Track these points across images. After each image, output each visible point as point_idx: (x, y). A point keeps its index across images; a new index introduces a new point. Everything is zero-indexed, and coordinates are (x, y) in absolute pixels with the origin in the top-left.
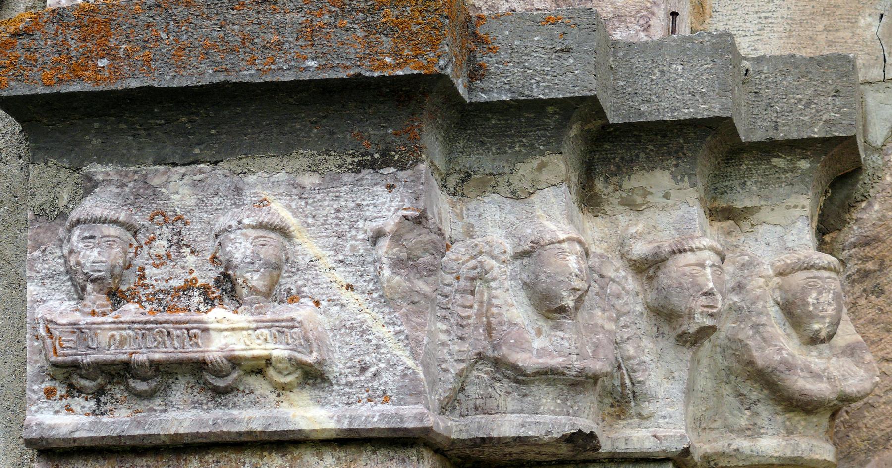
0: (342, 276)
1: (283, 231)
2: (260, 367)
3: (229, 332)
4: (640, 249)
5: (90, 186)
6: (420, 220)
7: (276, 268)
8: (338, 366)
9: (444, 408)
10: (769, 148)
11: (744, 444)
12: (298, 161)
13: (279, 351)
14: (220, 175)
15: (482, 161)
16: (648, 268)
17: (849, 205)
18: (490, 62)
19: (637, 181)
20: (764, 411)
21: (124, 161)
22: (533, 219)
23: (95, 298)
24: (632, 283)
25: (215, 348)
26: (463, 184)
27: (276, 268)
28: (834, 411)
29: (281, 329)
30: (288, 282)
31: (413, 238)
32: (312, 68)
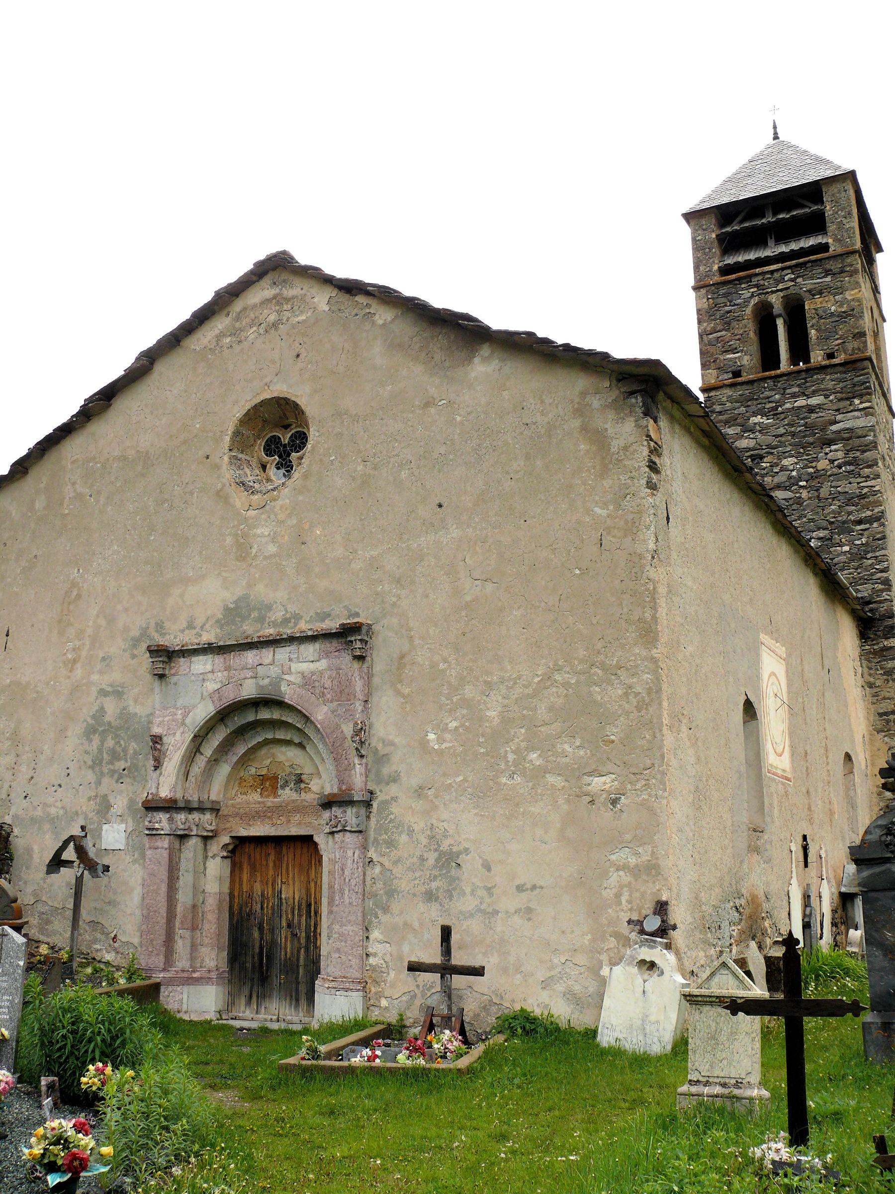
3: (157, 826)
22: (181, 817)
26: (177, 813)
28: (212, 831)
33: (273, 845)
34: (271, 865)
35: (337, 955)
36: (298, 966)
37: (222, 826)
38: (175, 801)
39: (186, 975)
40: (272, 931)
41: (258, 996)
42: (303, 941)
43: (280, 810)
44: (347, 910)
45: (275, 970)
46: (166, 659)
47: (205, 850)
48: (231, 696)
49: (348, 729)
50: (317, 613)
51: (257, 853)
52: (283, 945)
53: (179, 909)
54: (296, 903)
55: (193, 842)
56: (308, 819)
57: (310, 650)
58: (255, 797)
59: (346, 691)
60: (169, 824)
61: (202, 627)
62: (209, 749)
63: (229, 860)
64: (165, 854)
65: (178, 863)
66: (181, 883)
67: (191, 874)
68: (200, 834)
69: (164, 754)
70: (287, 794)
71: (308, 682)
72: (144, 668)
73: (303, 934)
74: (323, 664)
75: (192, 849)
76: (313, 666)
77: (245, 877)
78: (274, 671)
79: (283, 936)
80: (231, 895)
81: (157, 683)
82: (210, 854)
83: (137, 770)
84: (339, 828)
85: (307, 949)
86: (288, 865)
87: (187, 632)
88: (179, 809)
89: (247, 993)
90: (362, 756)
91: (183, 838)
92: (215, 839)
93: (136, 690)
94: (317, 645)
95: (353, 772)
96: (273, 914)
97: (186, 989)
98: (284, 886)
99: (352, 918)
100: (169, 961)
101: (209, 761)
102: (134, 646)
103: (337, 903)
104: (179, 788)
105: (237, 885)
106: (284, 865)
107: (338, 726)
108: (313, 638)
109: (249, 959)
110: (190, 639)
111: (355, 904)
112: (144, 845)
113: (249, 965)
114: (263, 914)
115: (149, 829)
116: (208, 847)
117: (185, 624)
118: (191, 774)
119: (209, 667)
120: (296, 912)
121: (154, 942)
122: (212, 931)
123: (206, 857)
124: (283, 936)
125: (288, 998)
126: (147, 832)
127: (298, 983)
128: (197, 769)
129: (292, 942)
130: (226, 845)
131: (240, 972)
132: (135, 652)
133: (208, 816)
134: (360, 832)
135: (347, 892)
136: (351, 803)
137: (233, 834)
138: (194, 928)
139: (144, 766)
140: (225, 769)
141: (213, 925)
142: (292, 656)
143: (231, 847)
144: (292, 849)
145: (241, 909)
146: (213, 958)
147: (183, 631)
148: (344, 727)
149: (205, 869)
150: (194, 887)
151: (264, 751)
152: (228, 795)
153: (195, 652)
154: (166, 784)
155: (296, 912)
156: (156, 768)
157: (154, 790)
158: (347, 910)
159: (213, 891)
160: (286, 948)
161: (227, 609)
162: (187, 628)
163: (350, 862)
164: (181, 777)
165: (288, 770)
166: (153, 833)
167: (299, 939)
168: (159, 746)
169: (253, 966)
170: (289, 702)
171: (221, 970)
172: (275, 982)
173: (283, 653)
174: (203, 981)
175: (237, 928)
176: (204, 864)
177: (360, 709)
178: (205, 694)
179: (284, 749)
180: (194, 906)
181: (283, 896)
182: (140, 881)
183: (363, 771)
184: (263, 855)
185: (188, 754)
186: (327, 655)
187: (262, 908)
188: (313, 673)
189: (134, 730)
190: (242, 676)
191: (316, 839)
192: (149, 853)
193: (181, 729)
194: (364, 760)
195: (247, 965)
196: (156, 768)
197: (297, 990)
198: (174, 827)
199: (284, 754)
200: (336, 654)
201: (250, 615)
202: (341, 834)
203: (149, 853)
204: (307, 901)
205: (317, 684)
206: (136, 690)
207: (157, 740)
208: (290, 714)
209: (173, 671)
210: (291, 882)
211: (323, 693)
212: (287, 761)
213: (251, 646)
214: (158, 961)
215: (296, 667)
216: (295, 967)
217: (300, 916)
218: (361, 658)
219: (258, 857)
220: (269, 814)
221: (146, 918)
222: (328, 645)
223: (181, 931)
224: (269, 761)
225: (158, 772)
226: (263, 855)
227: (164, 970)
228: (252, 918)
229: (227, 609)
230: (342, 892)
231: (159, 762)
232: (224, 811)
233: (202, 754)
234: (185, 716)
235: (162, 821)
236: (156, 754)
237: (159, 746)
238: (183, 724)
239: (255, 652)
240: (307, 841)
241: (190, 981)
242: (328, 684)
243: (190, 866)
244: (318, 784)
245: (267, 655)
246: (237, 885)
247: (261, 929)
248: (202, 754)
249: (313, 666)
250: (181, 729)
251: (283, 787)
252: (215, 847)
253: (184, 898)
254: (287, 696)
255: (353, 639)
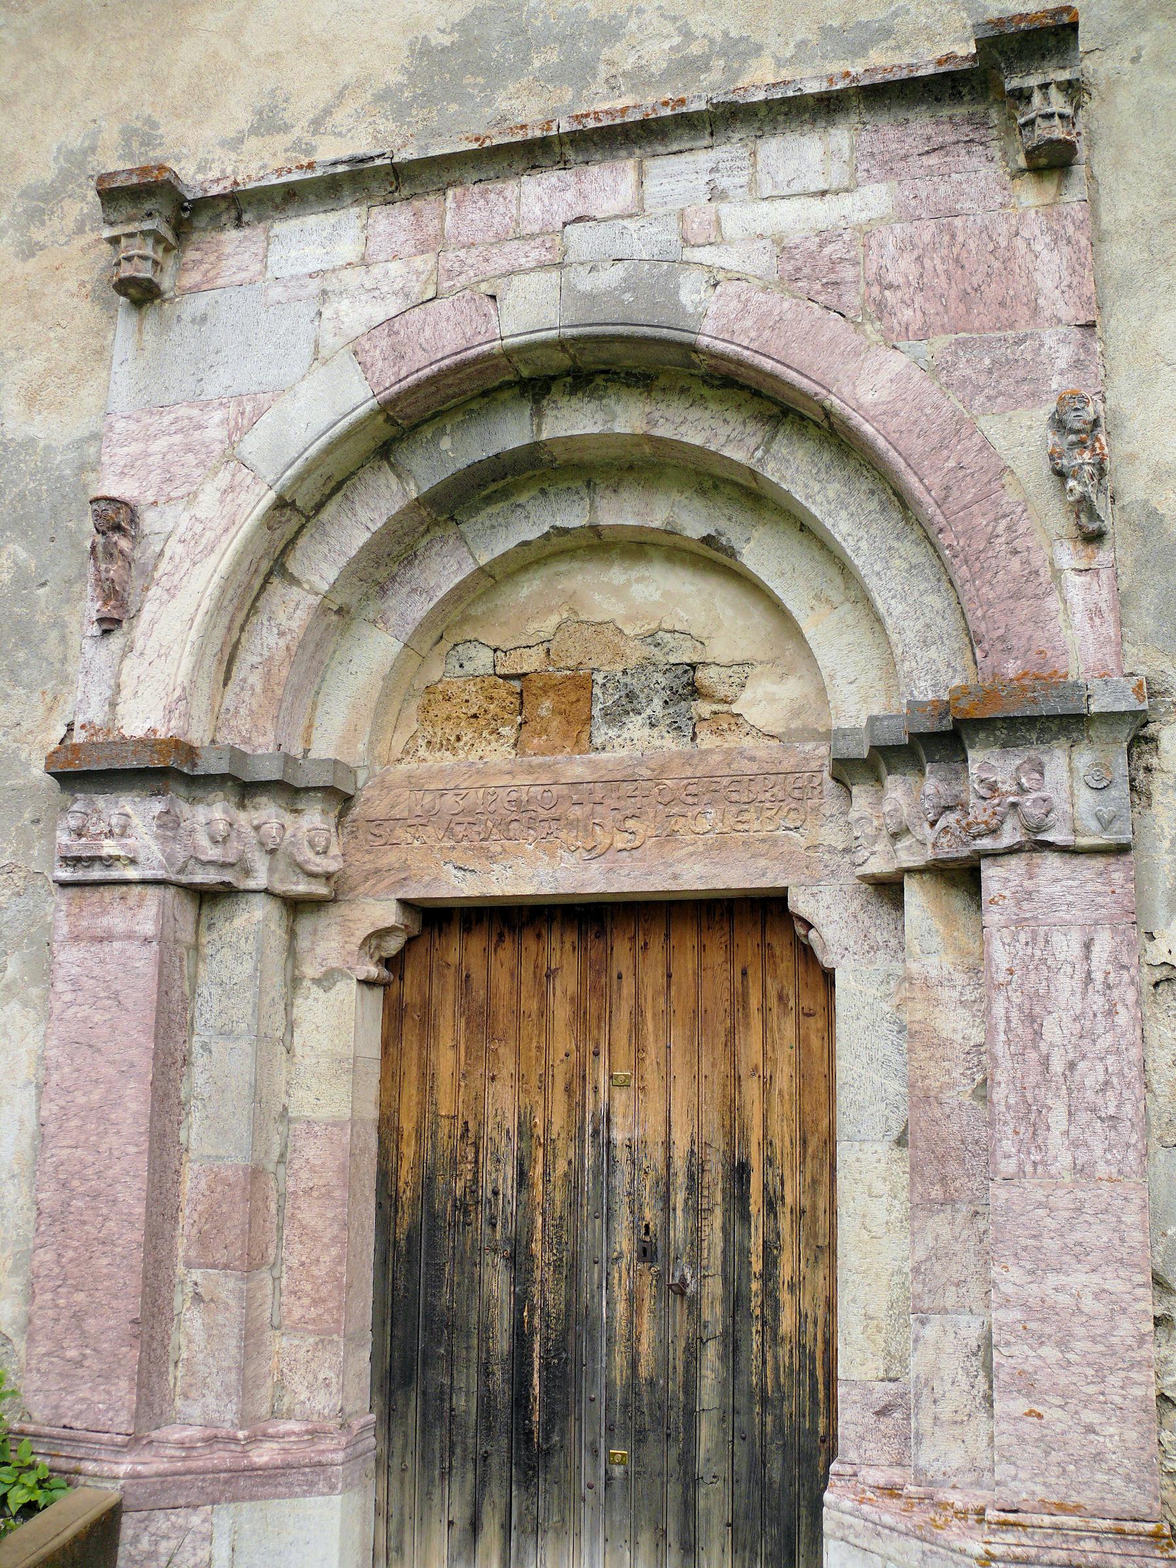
0: (144, 830)
1: (127, 815)
2: (118, 858)
3: (109, 847)
4: (255, 822)
5: (76, 800)
6: (167, 812)
7: (124, 828)
8: (141, 858)
9: (178, 873)
10: (307, 790)
11: (294, 887)
12: (134, 793)
13: (122, 854)
14: (111, 797)
15: (199, 793)
16: (257, 828)
17: (349, 808)
18: (199, 762)
19: (257, 800)
20: (301, 876)
21: (86, 792)
22: (214, 812)
23: (74, 836)
24: (253, 833)
25: (104, 852)
26: (194, 801)
27: (124, 828)
28: (328, 876)
29: (123, 846)
30: (129, 832)
31: (165, 818)
32: (135, 764)
33: (571, 938)
34: (561, 1011)
35: (1020, 1405)
36: (691, 1415)
37: (363, 861)
38: (191, 752)
39: (221, 1457)
40: (570, 1271)
41: (506, 1528)
42: (713, 1313)
43: (624, 790)
44: (1062, 1200)
45: (590, 1422)
46: (166, 232)
47: (292, 952)
48: (448, 336)
49: (1022, 437)
50: (826, 32)
51: (495, 966)
52: (620, 1326)
53: (192, 1183)
54: (680, 1164)
55: (254, 918)
56: (757, 827)
57: (806, 155)
58: (496, 753)
59: (992, 292)
60: (163, 840)
61: (316, 124)
62: (323, 564)
63: (379, 993)
64: (144, 960)
65: (187, 1002)
66: (199, 1078)
67: (245, 1045)
68: (279, 888)
69: (148, 574)
70: (633, 742)
71: (806, 270)
72: (72, 285)
73: (714, 1287)
74: (874, 199)
75: (249, 947)
76: (822, 212)
77: (445, 1060)
78: (643, 240)
79: (620, 1294)
80: (388, 1128)
81: (125, 322)
82: (310, 970)
83: (25, 641)
84: (1010, 836)
85: (733, 1347)
86: (638, 1012)
87: (252, 143)
88: (199, 784)
89: (459, 1511)
90: (1094, 538)
91: (209, 898)
92: (334, 911)
93: (36, 364)
94: (841, 137)
95: (1052, 603)
96: (573, 1205)
97: (224, 1518)
98: (621, 1098)
99: (1097, 1234)
100: (151, 1403)
101: (322, 610)
102: (36, 216)
103: (1008, 1167)
104: (200, 704)
105: (411, 1091)
106: (623, 1018)
107: (961, 426)
108: (826, 107)
109: (467, 1380)
110: (260, 165)
111: (1102, 1170)
112: (49, 928)
113: (465, 1404)
114: (525, 1206)
115: (77, 860)
116: (303, 943)
117: (244, 119)
118: (247, 658)
119: (348, 249)
120: (679, 1198)
121: (91, 1324)
122: (320, 1271)
123: (294, 982)
124: (620, 1294)
125: (646, 1538)
126: (65, 874)
127: (691, 1481)
128: (272, 639)
129: (662, 1318)
130: (382, 934)
131: (426, 1428)
132: (38, 235)
133: (314, 818)
134: (1121, 850)
135: (1058, 1118)
136: (1071, 724)
137: (414, 892)
138: (252, 1263)
139: (58, 624)
140: (376, 650)
141: (327, 1252)
142: (723, 182)
143: (393, 945)
144: (656, 951)
145: (428, 1183)
146: (325, 1378)
147: (235, 143)
148: (991, 427)
149: (291, 1026)
150: (257, 1095)
151: (529, 588)
152: (381, 749)
153: (288, 198)
154: (149, 690)
155: (679, 1198)
156: (109, 626)
157: (96, 713)
158: (1062, 1200)
159: (323, 1113)
160: (633, 1339)
161: (423, 51)
162: (255, 131)
163: (1066, 986)
164: (210, 663)
165: (636, 653)
166: (87, 877)
167: (694, 1305)
168: (124, 544)
169: (486, 1408)
170: (720, 346)
171: (356, 1424)
172: (589, 1472)
173: (677, 177)
174: (295, 1477)
175: (411, 1257)
176: (289, 1007)
177: (1065, 355)
178: (329, 341)
179: (617, 574)
180: (255, 1174)
181: (619, 1136)
182: (26, 1070)
183: (1103, 596)
184: (527, 974)
185: (241, 577)
186: (888, 167)
187: (522, 1178)
188: (824, 237)
189: (22, 497)
190: (500, 263)
191: (799, 903)
192: (69, 958)
193: (224, 478)
194: (1103, 555)
195: (460, 1402)
196: (109, 626)
197: (689, 1507)
198: (181, 855)
199: (619, 592)
200: (933, 160)
201: (526, 61)
202: (1016, 864)
203: (69, 958)
204: (729, 1155)
205: (848, 273)
206: (36, 364)
207: (116, 520)
208: (694, 413)
209: (193, 278)
210: (652, 1078)
211: (880, 305)
212: (631, 619)
213: (534, 153)
214: (109, 1403)
215: (737, 217)
216: (676, 1417)
217: (697, 1212)
218: (1052, 162)
219: (503, 985)
220: (577, 812)
221: (52, 1220)
222: (891, 133)
223: (197, 1275)
224: (554, 620)
225: (116, 642)
226: (527, 974)
227: (134, 1441)
228: (480, 1220)
229: (423, 51)
230: (1032, 1117)
231: (123, 605)
232: (372, 803)
233: (294, 581)
234: (237, 431)
235: (134, 828)
236: (114, 570)
237: (124, 544)
238: (231, 456)
239: (552, 178)
240: (767, 910)
241: (244, 1482)
242: (902, 269)
243: (241, 1011)
244: (772, 699)
245: (610, 184)
246: (411, 1091)
247: (518, 1259)
248: (294, 581)
249: (822, 212)
250: (224, 478)
251: (614, 717)
252: (334, 943)
253: (212, 1141)
254: (708, 326)
255: (1033, 81)
